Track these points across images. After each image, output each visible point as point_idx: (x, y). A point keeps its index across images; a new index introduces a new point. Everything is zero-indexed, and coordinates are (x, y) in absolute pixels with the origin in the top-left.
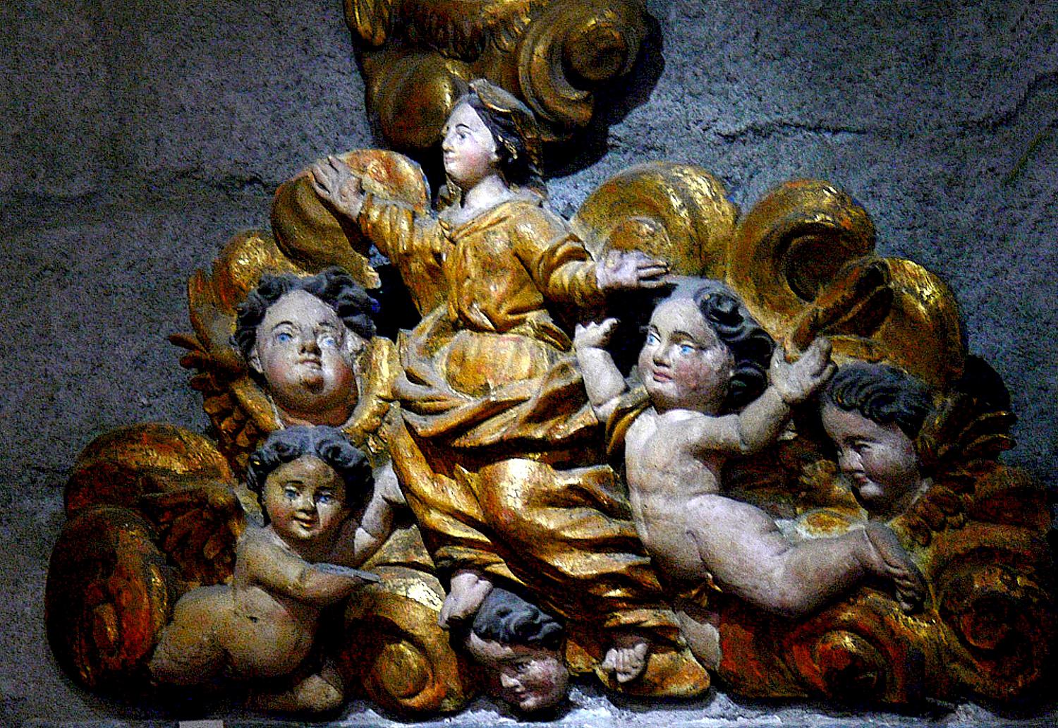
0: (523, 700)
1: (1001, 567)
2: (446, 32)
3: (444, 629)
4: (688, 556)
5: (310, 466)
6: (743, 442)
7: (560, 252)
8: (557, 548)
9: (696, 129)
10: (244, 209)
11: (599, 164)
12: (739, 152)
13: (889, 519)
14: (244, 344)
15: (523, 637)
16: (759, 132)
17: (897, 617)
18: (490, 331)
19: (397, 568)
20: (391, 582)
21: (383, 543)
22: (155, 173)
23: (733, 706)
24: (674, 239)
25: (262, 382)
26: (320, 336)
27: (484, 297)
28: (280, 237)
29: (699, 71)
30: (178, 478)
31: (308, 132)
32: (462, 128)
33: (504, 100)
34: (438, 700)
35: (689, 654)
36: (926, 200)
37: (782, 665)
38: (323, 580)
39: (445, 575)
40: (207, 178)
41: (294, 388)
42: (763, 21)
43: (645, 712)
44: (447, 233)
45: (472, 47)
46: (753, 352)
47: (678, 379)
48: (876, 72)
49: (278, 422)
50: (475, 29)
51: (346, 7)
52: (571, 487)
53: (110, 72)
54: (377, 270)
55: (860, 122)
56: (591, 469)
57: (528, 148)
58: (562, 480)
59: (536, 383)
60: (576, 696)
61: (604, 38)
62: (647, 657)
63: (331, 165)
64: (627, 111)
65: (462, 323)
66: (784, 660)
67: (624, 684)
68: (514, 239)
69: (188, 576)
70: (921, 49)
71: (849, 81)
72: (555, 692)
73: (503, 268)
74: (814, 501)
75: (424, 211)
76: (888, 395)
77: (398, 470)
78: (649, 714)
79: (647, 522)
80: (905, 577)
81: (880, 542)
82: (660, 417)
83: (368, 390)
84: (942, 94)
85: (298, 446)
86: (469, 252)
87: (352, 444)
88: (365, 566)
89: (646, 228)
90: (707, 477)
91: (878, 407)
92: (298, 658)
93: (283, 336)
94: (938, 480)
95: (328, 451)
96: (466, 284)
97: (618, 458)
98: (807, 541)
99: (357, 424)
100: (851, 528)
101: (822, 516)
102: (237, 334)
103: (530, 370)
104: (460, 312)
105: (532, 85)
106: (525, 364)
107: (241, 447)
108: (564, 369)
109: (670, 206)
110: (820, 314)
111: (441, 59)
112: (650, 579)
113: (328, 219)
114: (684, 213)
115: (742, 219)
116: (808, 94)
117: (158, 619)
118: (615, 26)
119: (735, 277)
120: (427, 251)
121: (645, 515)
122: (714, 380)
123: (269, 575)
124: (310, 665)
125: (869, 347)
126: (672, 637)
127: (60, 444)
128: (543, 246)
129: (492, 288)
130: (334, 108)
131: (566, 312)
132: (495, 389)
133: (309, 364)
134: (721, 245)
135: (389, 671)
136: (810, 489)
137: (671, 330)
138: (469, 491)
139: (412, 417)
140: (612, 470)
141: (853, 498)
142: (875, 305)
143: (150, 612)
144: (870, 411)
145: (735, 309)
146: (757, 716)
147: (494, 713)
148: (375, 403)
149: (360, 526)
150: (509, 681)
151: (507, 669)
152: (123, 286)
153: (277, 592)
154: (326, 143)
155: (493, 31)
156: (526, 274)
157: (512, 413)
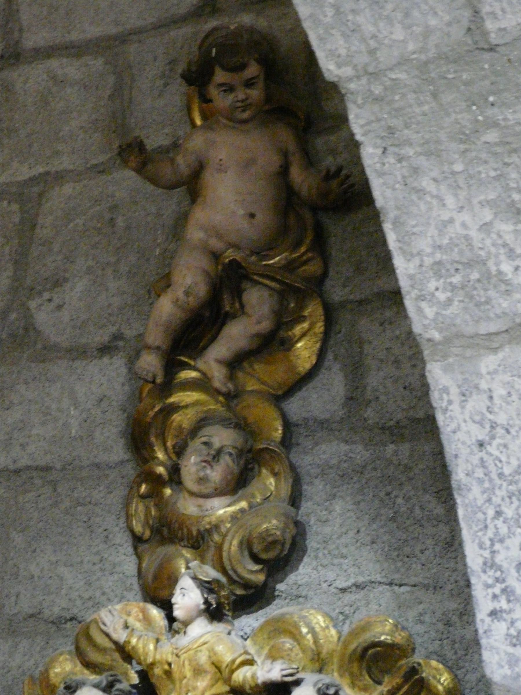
2: (183, 533)
9: (325, 585)
10: (67, 636)
11: (271, 606)
12: (348, 598)
16: (358, 586)
24: (304, 651)
29: (326, 552)
32: (183, 590)
33: (210, 573)
36: (448, 624)
42: (361, 524)
45: (197, 541)
54: (137, 672)
55: (413, 580)
57: (222, 600)
61: (272, 535)
64: (286, 575)
68: (212, 654)
70: (446, 539)
71: (408, 557)
73: (206, 672)
84: (457, 563)
86: (187, 663)
89: (288, 645)
96: (185, 681)
105: (231, 564)
109: (301, 632)
111: (180, 548)
113: (108, 644)
114: (309, 636)
115: (342, 639)
116: (386, 565)
118: (277, 528)
120: (164, 662)
128: (228, 658)
130: (121, 575)
134: (331, 654)
154: (116, 596)
155: (209, 532)
156: (219, 674)
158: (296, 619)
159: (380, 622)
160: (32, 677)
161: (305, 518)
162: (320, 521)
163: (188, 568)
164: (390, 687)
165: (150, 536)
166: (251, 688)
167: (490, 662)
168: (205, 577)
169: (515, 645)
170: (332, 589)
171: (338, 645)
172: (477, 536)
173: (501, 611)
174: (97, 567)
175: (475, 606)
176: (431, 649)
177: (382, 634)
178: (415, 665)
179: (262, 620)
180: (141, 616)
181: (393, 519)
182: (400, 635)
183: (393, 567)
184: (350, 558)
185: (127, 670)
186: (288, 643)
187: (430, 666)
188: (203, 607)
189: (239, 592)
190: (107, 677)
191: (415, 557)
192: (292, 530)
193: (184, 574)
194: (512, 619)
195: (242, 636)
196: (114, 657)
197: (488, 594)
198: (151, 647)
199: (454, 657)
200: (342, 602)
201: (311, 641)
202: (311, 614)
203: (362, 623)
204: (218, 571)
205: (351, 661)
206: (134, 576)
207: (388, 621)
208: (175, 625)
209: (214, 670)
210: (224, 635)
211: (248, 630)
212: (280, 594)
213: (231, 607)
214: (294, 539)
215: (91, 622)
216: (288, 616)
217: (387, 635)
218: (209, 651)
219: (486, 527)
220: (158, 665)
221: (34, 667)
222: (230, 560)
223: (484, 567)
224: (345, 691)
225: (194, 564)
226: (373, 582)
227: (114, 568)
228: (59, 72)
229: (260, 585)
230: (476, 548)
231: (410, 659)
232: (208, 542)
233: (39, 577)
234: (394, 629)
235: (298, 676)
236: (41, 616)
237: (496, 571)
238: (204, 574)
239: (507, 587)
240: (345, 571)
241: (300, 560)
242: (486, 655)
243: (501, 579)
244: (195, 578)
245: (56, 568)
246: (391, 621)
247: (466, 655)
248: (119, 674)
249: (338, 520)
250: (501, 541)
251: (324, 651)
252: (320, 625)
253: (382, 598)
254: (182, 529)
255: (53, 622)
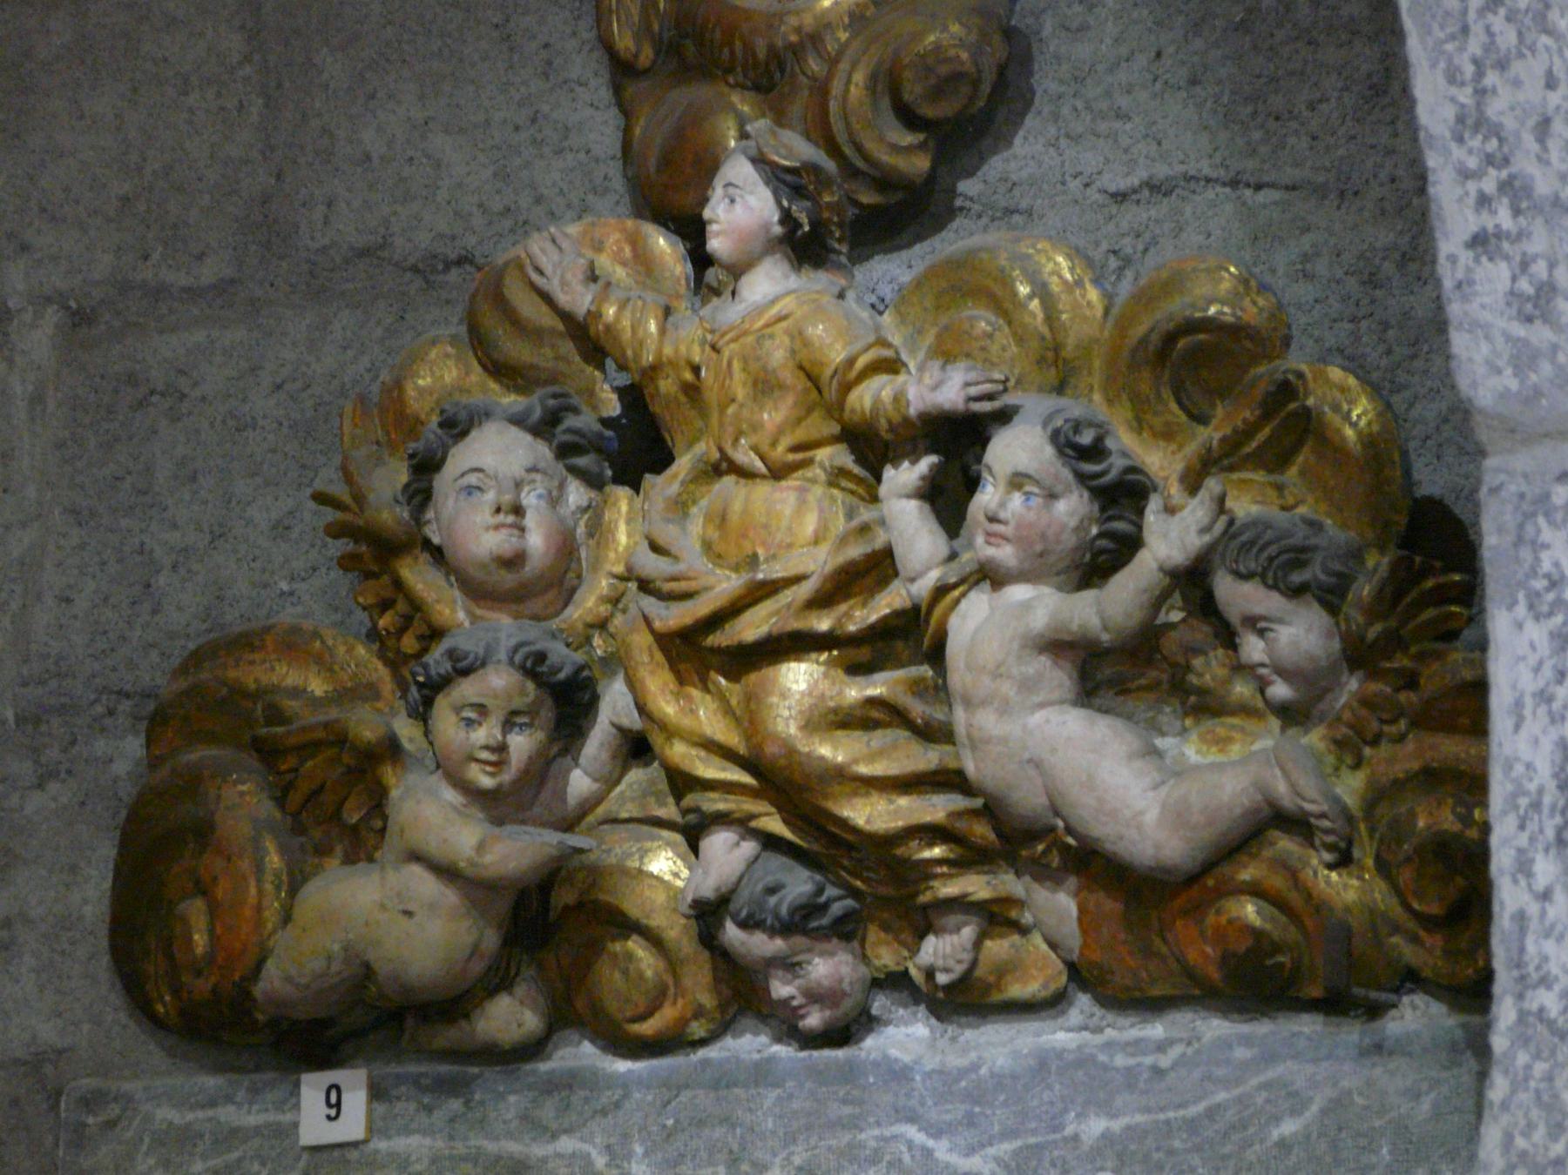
0: (803, 1017)
1: (1453, 796)
2: (732, 53)
3: (687, 917)
4: (1028, 798)
5: (498, 681)
6: (1105, 628)
7: (861, 362)
8: (848, 790)
9: (1075, 185)
10: (448, 302)
11: (944, 233)
12: (1131, 215)
13: (1306, 732)
14: (417, 500)
15: (801, 922)
16: (1157, 188)
17: (1315, 873)
18: (763, 477)
19: (630, 826)
20: (614, 848)
21: (610, 791)
22: (324, 250)
23: (1099, 1011)
24: (1020, 340)
25: (438, 554)
26: (526, 489)
27: (756, 427)
28: (478, 342)
29: (1080, 104)
30: (316, 703)
31: (545, 192)
32: (731, 190)
33: (796, 148)
34: (683, 1022)
35: (1037, 939)
36: (1372, 281)
37: (1164, 950)
38: (515, 851)
39: (693, 835)
40: (396, 257)
41: (483, 566)
43: (978, 1027)
44: (709, 337)
46: (1123, 496)
47: (1018, 540)
48: (1312, 107)
49: (461, 615)
50: (771, 48)
51: (601, 18)
52: (872, 702)
53: (267, 106)
55: (1290, 174)
56: (900, 674)
57: (826, 215)
58: (855, 691)
59: (823, 551)
60: (883, 1007)
61: (947, 60)
62: (978, 944)
63: (554, 241)
64: (982, 159)
65: (723, 467)
66: (1164, 939)
67: (948, 988)
69: (323, 851)
70: (1369, 76)
71: (1277, 119)
72: (847, 1005)
73: (782, 387)
74: (1204, 706)
75: (682, 306)
76: (1299, 556)
77: (631, 684)
78: (983, 1029)
79: (974, 748)
80: (1323, 816)
81: (1290, 766)
82: (995, 595)
83: (596, 566)
85: (481, 652)
86: (736, 365)
87: (568, 645)
88: (584, 824)
90: (1058, 677)
91: (1285, 576)
92: (477, 968)
93: (470, 490)
94: (1374, 674)
95: (526, 658)
96: (731, 410)
97: (936, 654)
98: (1197, 768)
99: (576, 616)
100: (1257, 746)
101: (1218, 730)
102: (407, 486)
103: (816, 532)
104: (721, 450)
105: (848, 124)
106: (810, 524)
107: (405, 655)
108: (864, 529)
109: (1015, 294)
110: (1215, 443)
111: (726, 89)
112: (982, 831)
113: (548, 319)
114: (1035, 304)
115: (1115, 311)
117: (271, 915)
118: (962, 44)
119: (1105, 390)
120: (682, 363)
121: (969, 736)
122: (1070, 540)
123: (433, 847)
124: (498, 980)
125: (1280, 488)
126: (1013, 914)
127: (154, 655)
128: (837, 355)
129: (766, 416)
130: (582, 156)
131: (872, 447)
132: (767, 560)
133: (504, 531)
134: (1086, 348)
135: (609, 982)
136: (1202, 692)
137: (1009, 470)
138: (728, 710)
139: (649, 604)
140: (931, 673)
141: (1260, 704)
142: (1285, 430)
143: (259, 909)
144: (1275, 578)
145: (1099, 440)
146: (1132, 1026)
147: (763, 1039)
148: (604, 583)
149: (577, 765)
150: (782, 989)
151: (780, 973)
152: (265, 417)
153: (446, 872)
154: (569, 206)
155: (797, 50)
156: (814, 394)
157: (787, 596)
158: (1003, 261)
159: (1208, 271)
160: (362, 399)
161: (1030, 20)
162: (1068, 29)
163: (743, 136)
164: (1228, 431)
165: (654, 62)
166: (892, 428)
167: (1470, 360)
168: (785, 158)
169: (1529, 319)
170: (1093, 195)
171: (1102, 329)
172: (1443, 52)
173: (1499, 234)
174: (524, 135)
175: (1437, 224)
176: (1330, 341)
177: (1210, 302)
178: (1290, 377)
179: (920, 267)
180: (627, 251)
181: (1243, 27)
182: (1254, 303)
183: (1240, 142)
184: (1137, 120)
185: (594, 382)
186: (982, 320)
187: (1327, 380)
188: (778, 230)
189: (867, 198)
190: (542, 401)
191: (1296, 118)
192: (997, 50)
193: (734, 150)
194: (1524, 254)
195: (873, 306)
196: (563, 351)
197: (1467, 194)
198: (653, 327)
199: (1384, 362)
200: (1117, 226)
201: (1040, 316)
202: (1038, 251)
203: (1165, 274)
204: (817, 144)
205: (1133, 366)
206: (613, 158)
207: (1227, 270)
208: (711, 275)
209: (802, 383)
210: (827, 300)
211: (887, 291)
212: (968, 204)
213: (848, 233)
214: (1002, 70)
215: (507, 264)
216: (985, 256)
217: (1223, 303)
218: (792, 338)
219: (1465, 30)
220: (669, 370)
221: (367, 377)
222: (846, 118)
223: (1460, 127)
224: (1117, 438)
225: (760, 126)
226: (1192, 177)
227: (566, 138)
228: (552, 1115)
229: (918, 181)
230: (1441, 81)
231: (1277, 362)
232: (793, 75)
233: (382, 158)
234: (1241, 289)
235: (1009, 399)
236: (386, 254)
237: (1486, 138)
238: (783, 151)
239: (1512, 177)
240: (1126, 151)
241: (1017, 120)
242: (1459, 342)
243: (1499, 155)
244: (759, 161)
245: (423, 137)
246: (1232, 269)
247: (1414, 357)
248: (572, 391)
249: (1111, 29)
250: (1502, 65)
251: (1071, 342)
252: (1060, 277)
253: (1212, 218)
254: (731, 44)
255: (415, 269)
